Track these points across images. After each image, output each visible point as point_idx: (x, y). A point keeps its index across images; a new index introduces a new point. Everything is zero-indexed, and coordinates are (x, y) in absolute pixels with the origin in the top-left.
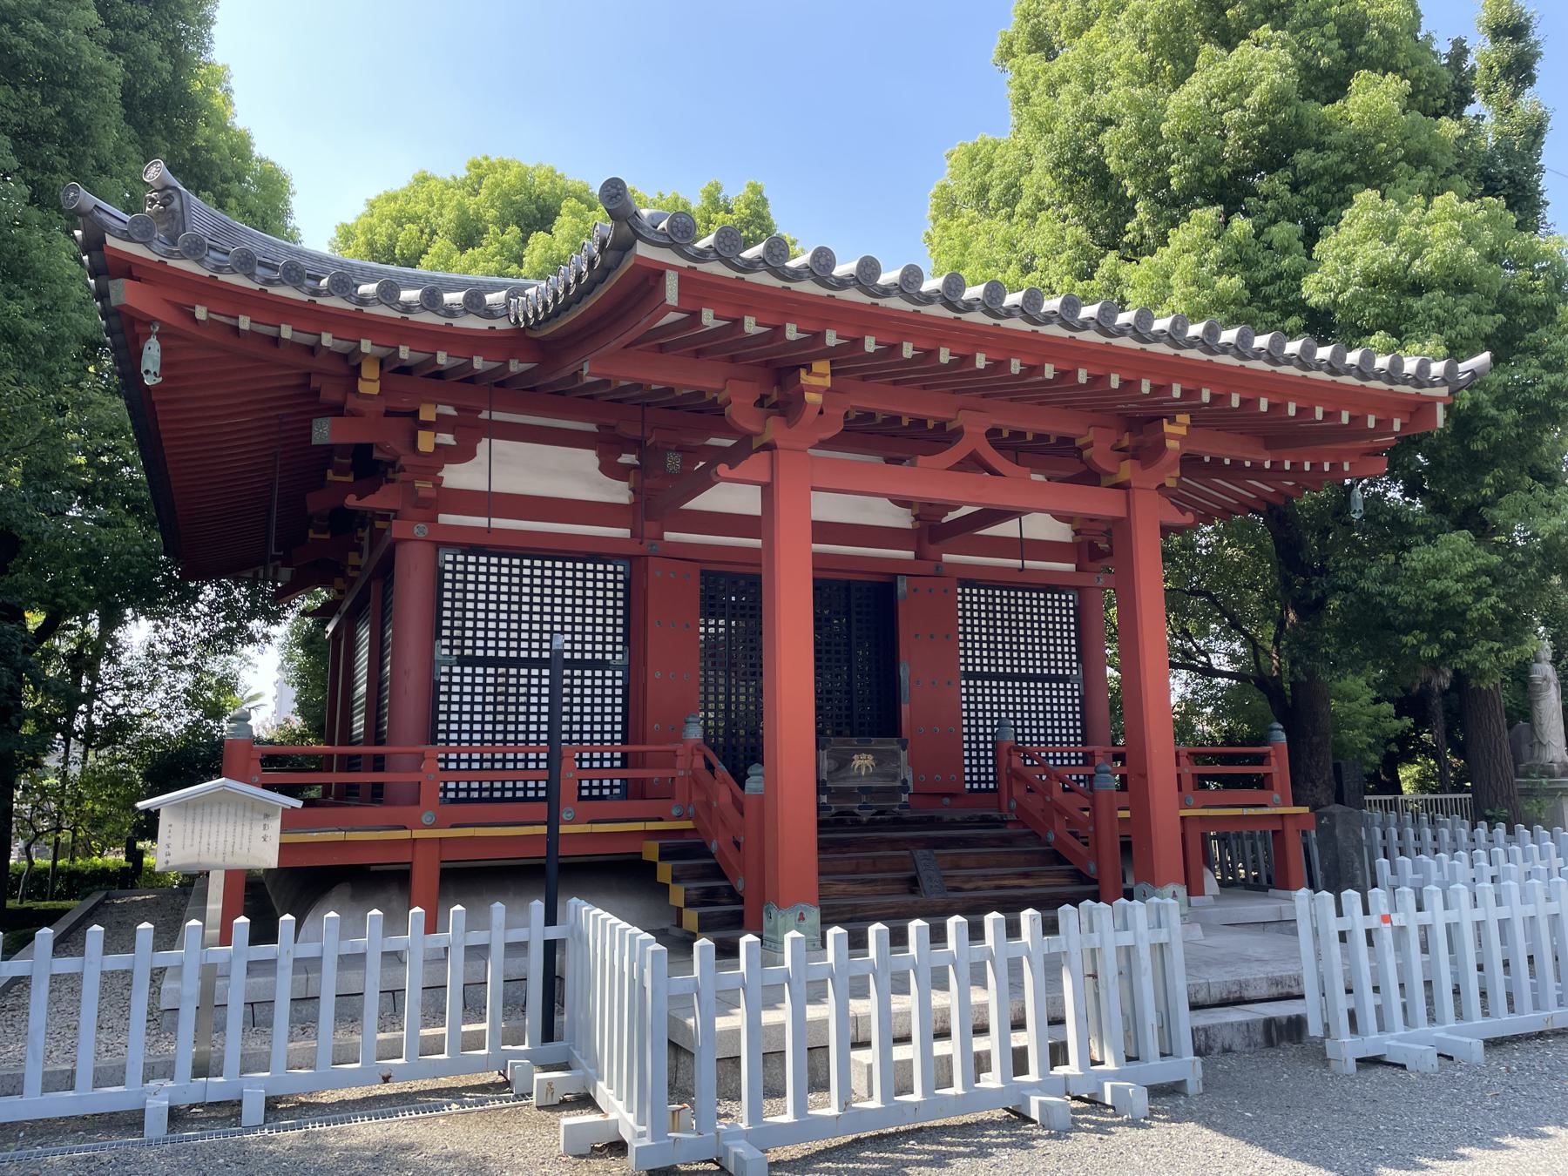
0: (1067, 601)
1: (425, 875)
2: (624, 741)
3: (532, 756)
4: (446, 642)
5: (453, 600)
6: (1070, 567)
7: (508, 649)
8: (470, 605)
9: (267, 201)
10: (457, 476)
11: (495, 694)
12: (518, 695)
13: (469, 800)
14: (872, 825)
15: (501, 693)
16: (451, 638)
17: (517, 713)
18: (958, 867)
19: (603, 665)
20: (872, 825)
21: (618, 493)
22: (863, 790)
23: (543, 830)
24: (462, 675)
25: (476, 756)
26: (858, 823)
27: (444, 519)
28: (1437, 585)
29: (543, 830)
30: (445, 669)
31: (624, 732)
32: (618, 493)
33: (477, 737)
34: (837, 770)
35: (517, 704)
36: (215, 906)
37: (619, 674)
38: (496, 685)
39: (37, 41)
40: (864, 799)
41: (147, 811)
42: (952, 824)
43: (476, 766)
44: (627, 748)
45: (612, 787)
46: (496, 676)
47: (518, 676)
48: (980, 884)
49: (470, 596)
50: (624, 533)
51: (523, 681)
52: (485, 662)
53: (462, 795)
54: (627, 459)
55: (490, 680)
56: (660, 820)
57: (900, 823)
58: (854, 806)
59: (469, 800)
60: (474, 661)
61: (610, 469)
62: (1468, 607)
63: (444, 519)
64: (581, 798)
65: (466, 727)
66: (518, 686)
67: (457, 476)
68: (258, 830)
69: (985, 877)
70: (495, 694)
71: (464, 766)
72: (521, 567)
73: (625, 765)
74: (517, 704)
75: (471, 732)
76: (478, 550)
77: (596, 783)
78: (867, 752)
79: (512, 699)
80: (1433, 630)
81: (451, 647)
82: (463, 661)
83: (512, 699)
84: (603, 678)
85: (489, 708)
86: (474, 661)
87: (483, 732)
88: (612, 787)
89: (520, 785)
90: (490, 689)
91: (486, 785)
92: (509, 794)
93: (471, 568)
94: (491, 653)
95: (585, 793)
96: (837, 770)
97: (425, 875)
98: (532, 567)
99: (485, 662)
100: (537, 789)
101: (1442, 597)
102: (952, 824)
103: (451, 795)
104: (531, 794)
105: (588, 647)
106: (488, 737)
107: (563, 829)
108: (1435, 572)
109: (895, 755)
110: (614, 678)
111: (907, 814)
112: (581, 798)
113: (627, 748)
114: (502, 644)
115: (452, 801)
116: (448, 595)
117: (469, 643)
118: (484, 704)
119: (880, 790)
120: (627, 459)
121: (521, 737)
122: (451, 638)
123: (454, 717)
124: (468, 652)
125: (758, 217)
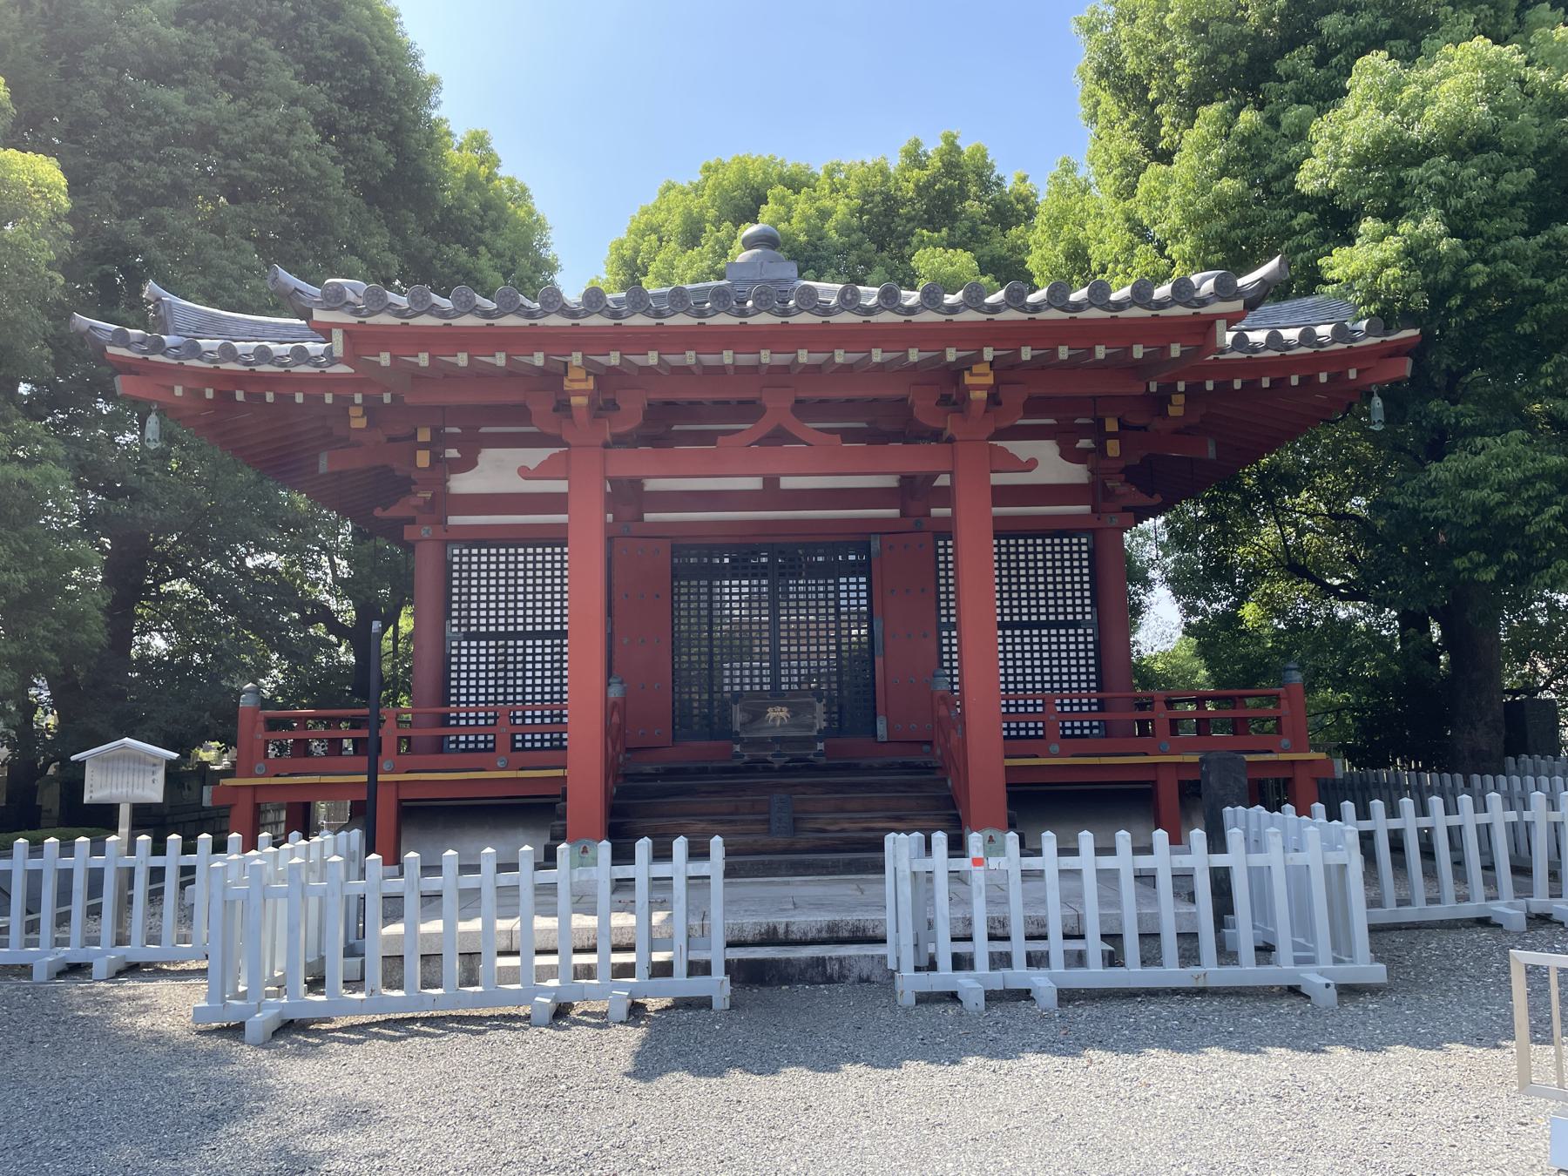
0: (1079, 544)
1: (1168, 792)
2: (1099, 689)
3: (529, 713)
4: (455, 622)
5: (460, 586)
6: (1086, 509)
7: (534, 624)
8: (520, 589)
9: (525, 266)
10: (462, 484)
11: (496, 663)
12: (515, 662)
13: (476, 750)
14: (784, 771)
15: (502, 662)
16: (459, 617)
17: (515, 678)
18: (843, 811)
19: (1075, 624)
20: (784, 771)
21: (1076, 474)
22: (776, 739)
23: (364, 778)
24: (469, 648)
25: (547, 713)
26: (771, 770)
27: (454, 520)
28: (1475, 495)
29: (364, 778)
30: (455, 644)
31: (1099, 681)
32: (1076, 474)
33: (482, 698)
34: (751, 721)
35: (515, 670)
36: (124, 829)
37: (1089, 631)
38: (496, 655)
39: (262, 169)
40: (778, 747)
41: (76, 762)
42: (870, 770)
43: (482, 722)
44: (444, 710)
45: (1091, 728)
46: (496, 647)
47: (515, 647)
48: (846, 826)
49: (521, 581)
50: (894, 512)
51: (520, 651)
52: (488, 636)
53: (471, 746)
54: (1084, 443)
55: (492, 651)
56: (1270, 752)
57: (810, 768)
58: (768, 755)
59: (476, 750)
60: (478, 636)
61: (1069, 454)
62: (1526, 520)
63: (454, 520)
64: (514, 749)
65: (473, 690)
66: (515, 655)
67: (462, 484)
68: (149, 780)
69: (852, 820)
70: (496, 663)
71: (472, 722)
72: (516, 555)
73: (1101, 709)
74: (515, 670)
75: (1025, 682)
76: (1061, 534)
77: (538, 737)
78: (782, 705)
79: (510, 666)
80: (1493, 552)
81: (459, 626)
82: (469, 636)
83: (510, 666)
84: (1076, 635)
85: (491, 674)
86: (478, 636)
87: (487, 694)
88: (1091, 728)
89: (471, 738)
90: (492, 659)
91: (1077, 724)
92: (1023, 733)
93: (1021, 549)
94: (1034, 618)
95: (519, 745)
96: (751, 721)
97: (1168, 792)
98: (1026, 545)
99: (488, 636)
100: (1036, 729)
101: (1484, 510)
102: (870, 770)
103: (462, 746)
104: (528, 745)
105: (1025, 610)
106: (529, 697)
107: (381, 778)
108: (1470, 483)
109: (812, 706)
110: (1085, 635)
111: (823, 761)
112: (1064, 736)
113: (444, 710)
114: (1043, 610)
115: (463, 750)
116: (456, 583)
117: (474, 621)
118: (487, 671)
119: (793, 740)
120: (1084, 443)
121: (519, 698)
122: (459, 617)
123: (463, 683)
124: (473, 629)
125: (1036, 196)
